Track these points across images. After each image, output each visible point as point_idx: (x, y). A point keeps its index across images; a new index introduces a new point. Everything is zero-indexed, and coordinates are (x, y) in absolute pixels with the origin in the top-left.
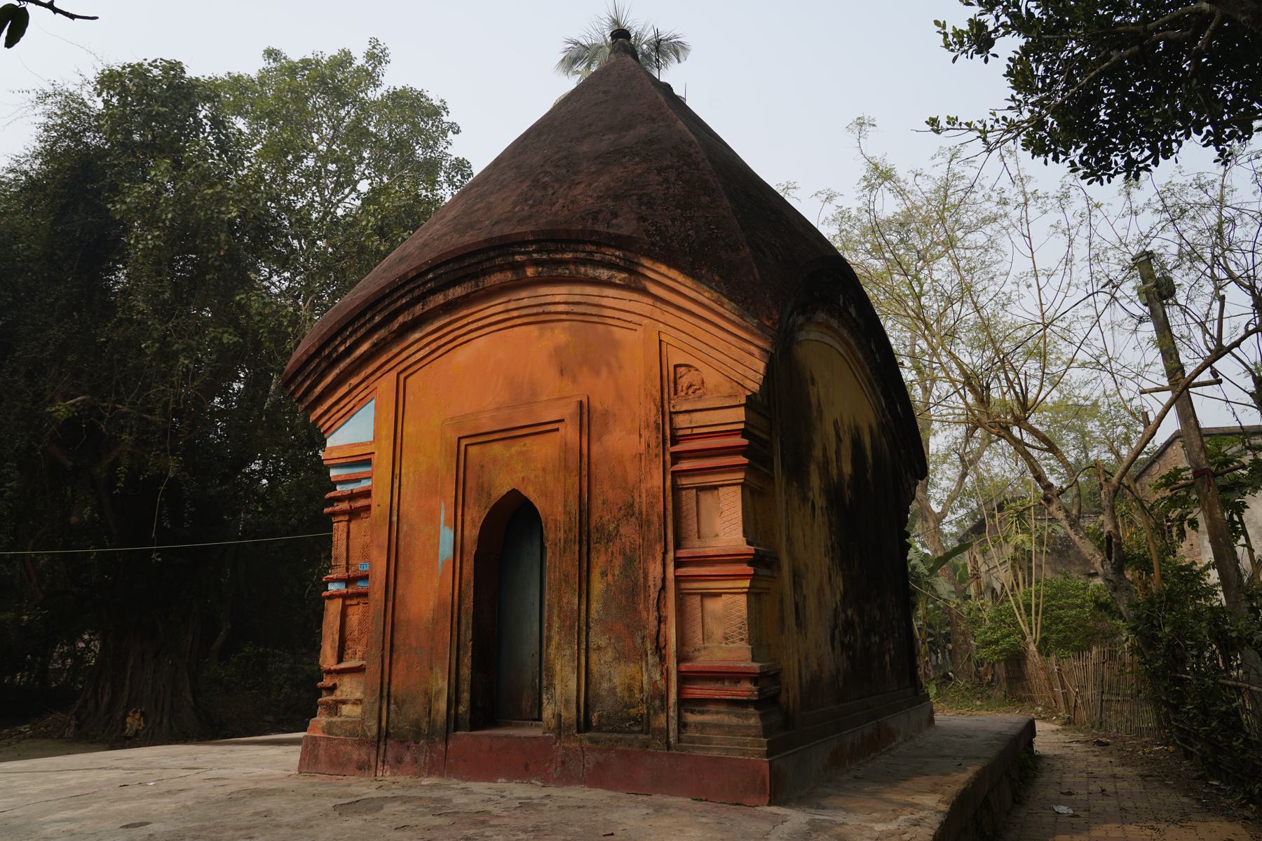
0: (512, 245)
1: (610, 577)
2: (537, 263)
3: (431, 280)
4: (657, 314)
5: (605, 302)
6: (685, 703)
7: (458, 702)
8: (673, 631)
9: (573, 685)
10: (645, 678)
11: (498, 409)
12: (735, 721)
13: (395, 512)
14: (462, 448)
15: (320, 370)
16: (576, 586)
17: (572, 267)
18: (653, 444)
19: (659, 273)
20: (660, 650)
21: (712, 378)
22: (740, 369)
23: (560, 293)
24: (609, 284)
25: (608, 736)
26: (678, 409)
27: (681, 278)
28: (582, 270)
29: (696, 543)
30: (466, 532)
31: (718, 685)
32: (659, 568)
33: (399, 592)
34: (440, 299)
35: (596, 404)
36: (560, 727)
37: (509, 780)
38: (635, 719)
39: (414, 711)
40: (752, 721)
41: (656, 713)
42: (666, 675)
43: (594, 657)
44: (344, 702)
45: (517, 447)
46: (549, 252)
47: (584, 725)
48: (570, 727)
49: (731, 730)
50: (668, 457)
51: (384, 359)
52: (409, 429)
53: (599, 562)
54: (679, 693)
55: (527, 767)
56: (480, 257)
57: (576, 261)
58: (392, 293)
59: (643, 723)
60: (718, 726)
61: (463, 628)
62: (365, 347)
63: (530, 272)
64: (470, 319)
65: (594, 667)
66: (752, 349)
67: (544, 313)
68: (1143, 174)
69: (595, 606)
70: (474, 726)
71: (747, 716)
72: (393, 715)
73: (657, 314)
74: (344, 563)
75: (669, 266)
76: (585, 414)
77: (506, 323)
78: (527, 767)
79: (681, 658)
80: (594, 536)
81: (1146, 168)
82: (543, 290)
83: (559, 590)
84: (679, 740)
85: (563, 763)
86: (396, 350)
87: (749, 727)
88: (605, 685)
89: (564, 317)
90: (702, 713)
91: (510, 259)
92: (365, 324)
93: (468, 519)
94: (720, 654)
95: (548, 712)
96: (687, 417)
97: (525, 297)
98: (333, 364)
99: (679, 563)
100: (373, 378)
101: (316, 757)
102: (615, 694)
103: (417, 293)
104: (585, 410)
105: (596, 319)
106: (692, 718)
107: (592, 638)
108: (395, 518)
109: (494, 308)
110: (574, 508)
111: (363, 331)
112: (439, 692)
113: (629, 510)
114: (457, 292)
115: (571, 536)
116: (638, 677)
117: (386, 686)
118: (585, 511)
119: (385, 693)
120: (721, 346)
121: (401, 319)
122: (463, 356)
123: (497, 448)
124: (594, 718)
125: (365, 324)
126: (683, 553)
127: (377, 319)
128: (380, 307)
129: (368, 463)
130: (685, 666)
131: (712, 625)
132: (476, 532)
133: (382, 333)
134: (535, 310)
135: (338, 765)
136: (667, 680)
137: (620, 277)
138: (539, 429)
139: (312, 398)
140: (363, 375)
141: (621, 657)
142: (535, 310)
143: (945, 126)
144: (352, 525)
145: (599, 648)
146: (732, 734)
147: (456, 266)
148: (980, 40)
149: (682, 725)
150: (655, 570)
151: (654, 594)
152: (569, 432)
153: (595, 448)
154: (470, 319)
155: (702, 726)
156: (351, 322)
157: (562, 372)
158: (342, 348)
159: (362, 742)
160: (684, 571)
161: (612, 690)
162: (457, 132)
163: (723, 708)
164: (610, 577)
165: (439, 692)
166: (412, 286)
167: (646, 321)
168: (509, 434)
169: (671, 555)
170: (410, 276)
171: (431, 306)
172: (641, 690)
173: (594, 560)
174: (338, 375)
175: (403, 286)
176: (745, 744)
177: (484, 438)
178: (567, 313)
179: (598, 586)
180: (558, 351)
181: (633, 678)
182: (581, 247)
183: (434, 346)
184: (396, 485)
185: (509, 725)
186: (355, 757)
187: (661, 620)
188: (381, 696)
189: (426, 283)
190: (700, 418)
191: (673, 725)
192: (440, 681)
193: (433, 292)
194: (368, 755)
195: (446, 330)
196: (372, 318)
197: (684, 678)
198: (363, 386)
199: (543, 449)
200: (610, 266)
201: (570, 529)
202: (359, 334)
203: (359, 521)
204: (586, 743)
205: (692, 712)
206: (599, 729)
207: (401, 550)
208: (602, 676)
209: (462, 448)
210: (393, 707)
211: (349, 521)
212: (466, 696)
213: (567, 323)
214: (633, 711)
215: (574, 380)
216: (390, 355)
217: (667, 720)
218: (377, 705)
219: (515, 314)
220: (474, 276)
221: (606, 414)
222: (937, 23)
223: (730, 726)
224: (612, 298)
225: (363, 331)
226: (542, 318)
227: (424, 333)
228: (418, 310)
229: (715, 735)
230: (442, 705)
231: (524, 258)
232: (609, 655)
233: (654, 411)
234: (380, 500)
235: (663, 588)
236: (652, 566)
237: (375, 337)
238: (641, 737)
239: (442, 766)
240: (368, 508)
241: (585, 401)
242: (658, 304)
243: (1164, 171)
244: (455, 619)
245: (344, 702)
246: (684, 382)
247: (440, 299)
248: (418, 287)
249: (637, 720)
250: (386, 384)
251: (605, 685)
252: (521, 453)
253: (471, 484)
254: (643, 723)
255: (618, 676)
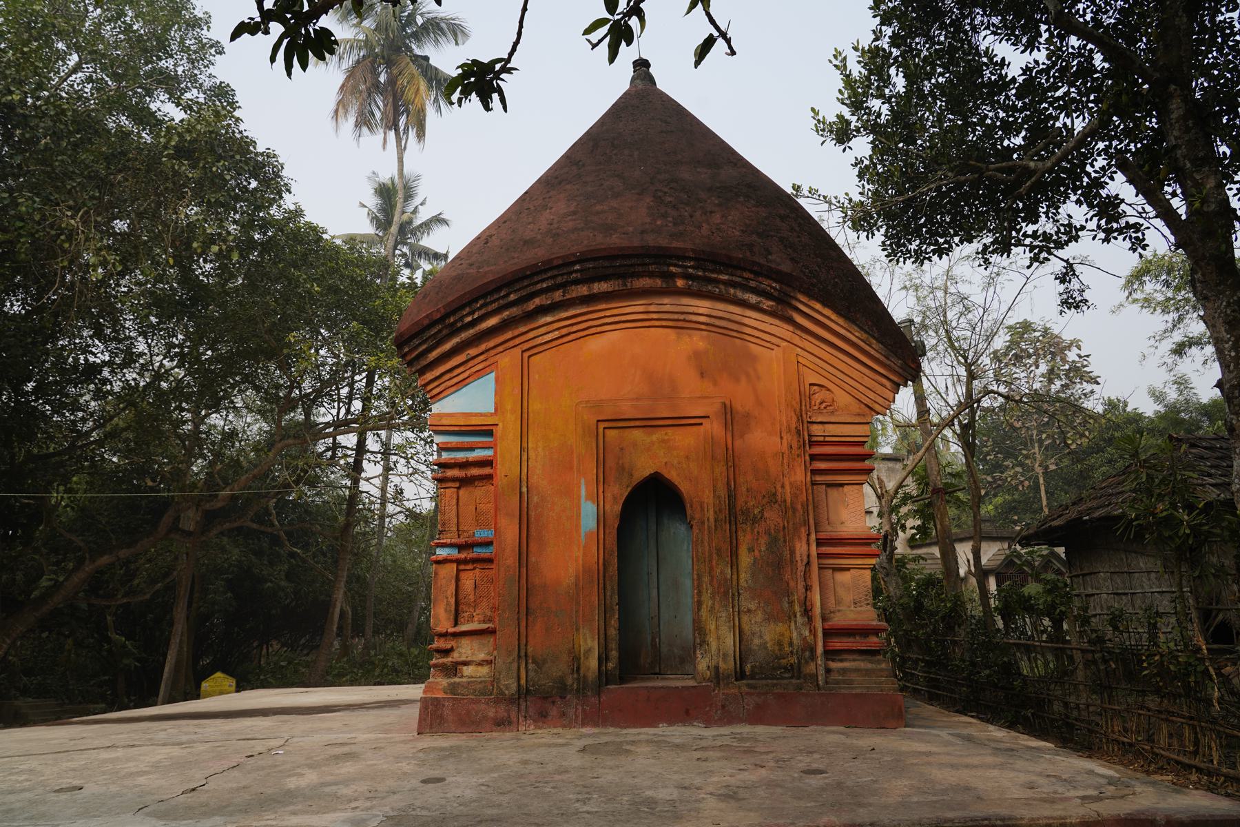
0: (670, 257)
1: (757, 552)
2: (687, 277)
3: (576, 271)
4: (797, 340)
5: (746, 321)
6: (830, 654)
7: (607, 659)
8: (818, 597)
9: (729, 641)
10: (795, 635)
11: (637, 399)
12: (870, 666)
13: (524, 484)
14: (601, 430)
15: (440, 336)
16: (728, 559)
17: (722, 287)
18: (795, 445)
19: (807, 304)
20: (807, 612)
21: (842, 398)
22: (872, 395)
23: (702, 306)
24: (756, 308)
25: (764, 682)
26: (814, 419)
27: (834, 317)
28: (732, 291)
29: (829, 528)
30: (608, 507)
31: (851, 639)
32: (805, 547)
33: (533, 559)
34: (583, 290)
35: (738, 406)
36: (717, 676)
37: (671, 724)
38: (785, 668)
39: (559, 668)
40: (883, 666)
41: (807, 662)
42: (813, 632)
43: (745, 618)
44: (465, 664)
45: (657, 435)
46: (705, 270)
47: (740, 675)
48: (728, 676)
49: (868, 672)
50: (808, 458)
51: (509, 335)
52: (535, 406)
53: (745, 539)
54: (824, 646)
55: (687, 712)
56: (633, 261)
57: (725, 283)
58: (533, 275)
59: (795, 671)
60: (857, 670)
61: (608, 593)
62: (492, 322)
63: (680, 283)
64: (608, 313)
65: (746, 627)
66: (884, 381)
67: (684, 320)
68: (926, 262)
69: (743, 576)
70: (622, 680)
71: (879, 662)
72: (531, 674)
73: (797, 340)
74: (454, 528)
75: (825, 305)
76: (729, 415)
77: (645, 323)
78: (687, 712)
79: (824, 619)
80: (740, 518)
81: (929, 259)
82: (685, 301)
83: (710, 561)
84: (827, 683)
85: (723, 707)
86: (523, 329)
87: (882, 670)
88: (757, 641)
89: (703, 327)
90: (841, 661)
91: (665, 268)
92: (498, 299)
93: (609, 495)
94: (852, 616)
95: (703, 664)
96: (820, 427)
97: (668, 303)
98: (455, 332)
99: (819, 543)
100: (493, 352)
101: (442, 717)
102: (766, 648)
103: (559, 280)
104: (728, 411)
105: (735, 334)
106: (833, 665)
107: (743, 603)
108: (524, 489)
109: (635, 307)
110: (723, 493)
111: (495, 306)
112: (589, 650)
113: (772, 498)
114: (603, 287)
115: (722, 516)
116: (787, 634)
117: (523, 647)
118: (732, 495)
119: (523, 654)
120: (855, 374)
121: (537, 301)
122: (595, 345)
123: (637, 434)
124: (748, 668)
125: (498, 299)
126: (822, 535)
127: (512, 297)
128: (517, 286)
129: (489, 433)
130: (828, 625)
131: (841, 592)
132: (618, 508)
133: (514, 311)
134: (676, 317)
135: (469, 723)
136: (815, 636)
137: (767, 304)
138: (679, 422)
139: (424, 362)
140: (483, 347)
141: (770, 618)
142: (676, 317)
143: (807, 194)
144: (461, 492)
145: (749, 611)
146: (870, 676)
147: (607, 264)
148: (842, 134)
149: (828, 671)
150: (801, 548)
151: (801, 567)
152: (714, 428)
153: (738, 443)
154: (608, 313)
155: (844, 671)
156: (484, 296)
157: (702, 375)
158: (469, 319)
159: (500, 699)
160: (825, 549)
161: (764, 646)
162: (220, 53)
163: (855, 657)
164: (757, 552)
165: (589, 650)
166: (555, 272)
167: (785, 344)
168: (649, 423)
169: (813, 537)
170: (555, 263)
171: (574, 295)
172: (791, 644)
173: (741, 538)
174: (458, 344)
175: (545, 271)
176: (881, 683)
177: (620, 423)
178: (707, 324)
179: (745, 559)
180: (697, 356)
181: (782, 635)
182: (739, 272)
183: (564, 331)
184: (525, 458)
185: (634, 679)
186: (491, 714)
187: (808, 588)
188: (519, 657)
189: (571, 273)
190: (831, 429)
191: (821, 671)
192: (589, 641)
193: (577, 282)
194: (508, 711)
195: (580, 319)
196: (508, 295)
197: (827, 633)
198: (482, 358)
199: (684, 439)
200: (768, 296)
201: (720, 511)
202: (490, 308)
203: (471, 489)
204: (745, 689)
205: (833, 660)
206: (752, 677)
207: (532, 520)
208: (753, 634)
209: (601, 430)
210: (531, 666)
211: (458, 488)
212: (614, 654)
213: (705, 333)
214: (784, 662)
215: (715, 383)
216: (516, 332)
217: (817, 667)
218: (516, 665)
219: (654, 316)
220: (622, 277)
221: (747, 416)
222: (813, 109)
223: (867, 670)
224: (752, 318)
225: (495, 306)
226: (682, 324)
227: (557, 317)
228: (558, 295)
229: (853, 676)
230: (594, 663)
231: (679, 270)
232: (759, 616)
233: (795, 419)
234: (507, 468)
235: (808, 563)
236: (798, 545)
237: (506, 314)
238: (794, 681)
239: (597, 718)
240: (489, 477)
241: (728, 403)
242: (799, 332)
243: (936, 267)
244: (601, 585)
245: (465, 664)
246: (818, 398)
247: (583, 290)
248: (562, 275)
249: (789, 669)
250: (508, 360)
251: (757, 641)
252: (663, 441)
253: (611, 462)
254: (795, 671)
255: (767, 634)
